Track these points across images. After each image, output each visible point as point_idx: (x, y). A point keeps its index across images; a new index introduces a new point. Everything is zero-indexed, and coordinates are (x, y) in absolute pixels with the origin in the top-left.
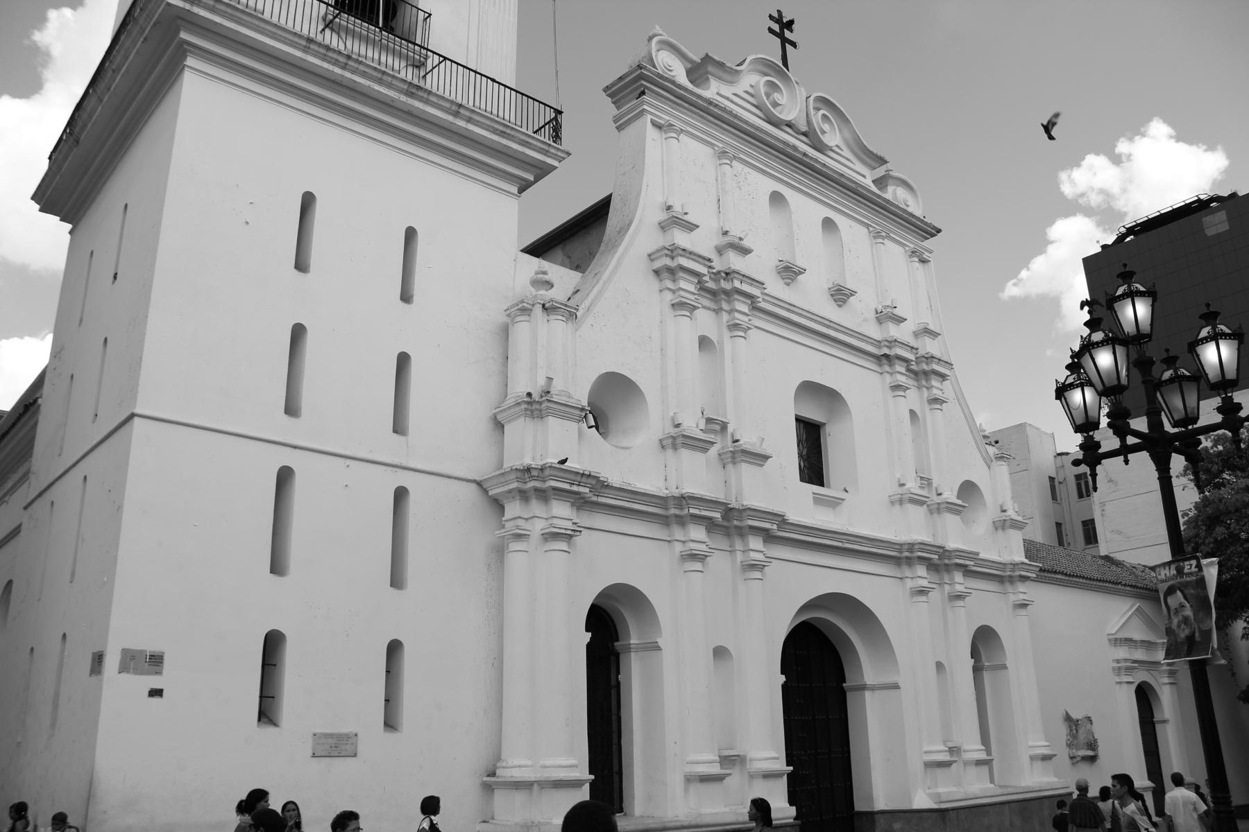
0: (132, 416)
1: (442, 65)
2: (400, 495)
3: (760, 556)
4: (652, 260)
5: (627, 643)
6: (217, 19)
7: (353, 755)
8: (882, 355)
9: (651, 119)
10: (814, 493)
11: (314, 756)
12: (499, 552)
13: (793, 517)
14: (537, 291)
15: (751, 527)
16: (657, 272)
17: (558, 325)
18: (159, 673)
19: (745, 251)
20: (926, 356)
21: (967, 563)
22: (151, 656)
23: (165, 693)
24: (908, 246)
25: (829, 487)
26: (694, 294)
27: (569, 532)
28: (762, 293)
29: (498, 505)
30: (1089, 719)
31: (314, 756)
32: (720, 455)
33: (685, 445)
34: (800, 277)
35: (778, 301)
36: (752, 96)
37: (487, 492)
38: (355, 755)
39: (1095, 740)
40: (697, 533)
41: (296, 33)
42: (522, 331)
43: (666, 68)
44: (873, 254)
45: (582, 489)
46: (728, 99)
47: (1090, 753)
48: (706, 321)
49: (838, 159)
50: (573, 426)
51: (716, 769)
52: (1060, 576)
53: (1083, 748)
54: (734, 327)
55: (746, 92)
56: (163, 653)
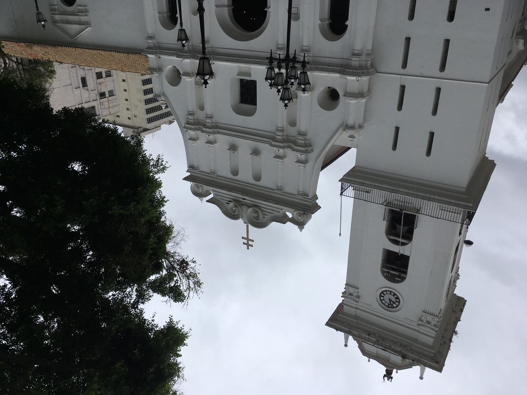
5: (161, 15)
10: (251, 77)
12: (373, 50)
16: (311, 146)
20: (196, 131)
29: (372, 66)
36: (265, 214)
37: (375, 69)
54: (282, 131)
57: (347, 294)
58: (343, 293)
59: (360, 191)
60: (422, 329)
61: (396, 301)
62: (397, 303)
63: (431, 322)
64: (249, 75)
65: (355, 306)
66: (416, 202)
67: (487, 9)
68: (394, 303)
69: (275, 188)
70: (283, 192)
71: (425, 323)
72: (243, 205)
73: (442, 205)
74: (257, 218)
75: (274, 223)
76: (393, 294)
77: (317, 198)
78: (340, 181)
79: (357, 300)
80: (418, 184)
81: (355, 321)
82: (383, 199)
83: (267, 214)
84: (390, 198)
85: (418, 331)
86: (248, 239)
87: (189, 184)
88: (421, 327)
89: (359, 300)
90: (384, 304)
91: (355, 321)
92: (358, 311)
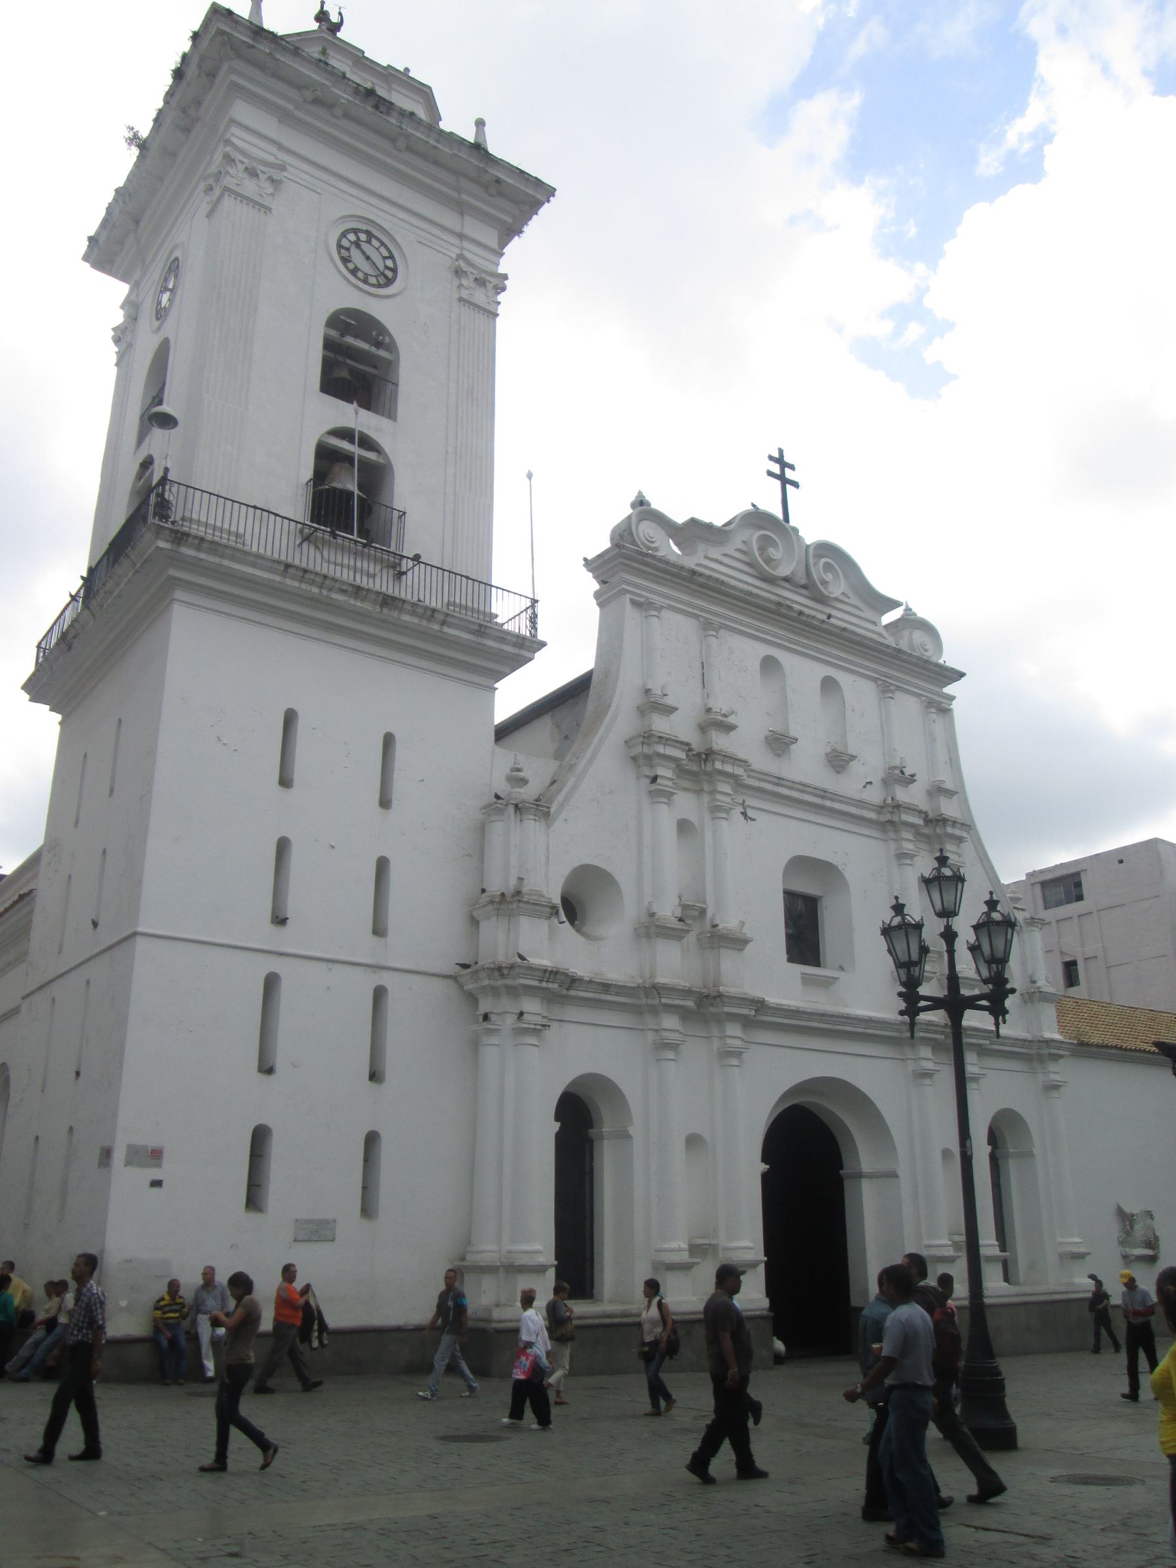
0: (135, 934)
1: (416, 568)
2: (379, 994)
3: (738, 1043)
4: (629, 747)
6: (250, 570)
7: (332, 1238)
8: (885, 822)
9: (630, 599)
10: (802, 974)
11: (296, 1240)
12: (475, 1045)
13: (772, 999)
14: (512, 788)
15: (727, 1014)
16: (634, 759)
17: (532, 826)
18: (159, 1166)
19: (730, 728)
21: (981, 1042)
22: (152, 1150)
23: (164, 1184)
24: (923, 696)
25: (825, 967)
26: (670, 779)
27: (538, 1027)
28: (745, 771)
29: (472, 999)
30: (1150, 1214)
31: (296, 1240)
32: (698, 940)
33: (658, 935)
34: (793, 747)
35: (765, 776)
37: (463, 987)
38: (333, 1240)
39: (1156, 1238)
40: (671, 1022)
41: (274, 561)
42: (497, 829)
43: (646, 539)
44: (880, 710)
45: (550, 985)
46: (717, 561)
47: (1150, 1252)
48: (686, 804)
49: (845, 609)
50: (544, 925)
51: (685, 1257)
52: (1113, 1051)
53: (1139, 1247)
55: (738, 550)
56: (163, 1148)
57: (492, 285)
58: (504, 289)
59: (460, 606)
60: (267, 153)
61: (348, 249)
62: (345, 243)
63: (245, 175)
64: (806, 980)
65: (466, 244)
66: (312, 558)
67: (1121, 862)
68: (357, 244)
69: (722, 632)
70: (699, 620)
71: (263, 172)
72: (804, 587)
73: (240, 546)
74: (765, 543)
75: (719, 522)
76: (360, 275)
77: (597, 595)
78: (543, 644)
79: (462, 264)
80: (289, 615)
81: (464, 197)
82: (410, 582)
83: (741, 557)
84: (385, 578)
85: (280, 147)
86: (784, 481)
87: (949, 658)
88: (271, 159)
89: (457, 263)
90: (383, 244)
91: (464, 197)
92: (458, 229)
